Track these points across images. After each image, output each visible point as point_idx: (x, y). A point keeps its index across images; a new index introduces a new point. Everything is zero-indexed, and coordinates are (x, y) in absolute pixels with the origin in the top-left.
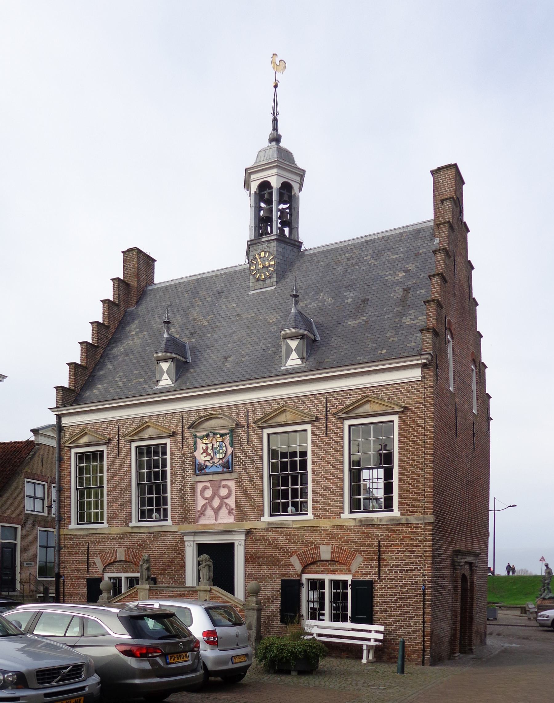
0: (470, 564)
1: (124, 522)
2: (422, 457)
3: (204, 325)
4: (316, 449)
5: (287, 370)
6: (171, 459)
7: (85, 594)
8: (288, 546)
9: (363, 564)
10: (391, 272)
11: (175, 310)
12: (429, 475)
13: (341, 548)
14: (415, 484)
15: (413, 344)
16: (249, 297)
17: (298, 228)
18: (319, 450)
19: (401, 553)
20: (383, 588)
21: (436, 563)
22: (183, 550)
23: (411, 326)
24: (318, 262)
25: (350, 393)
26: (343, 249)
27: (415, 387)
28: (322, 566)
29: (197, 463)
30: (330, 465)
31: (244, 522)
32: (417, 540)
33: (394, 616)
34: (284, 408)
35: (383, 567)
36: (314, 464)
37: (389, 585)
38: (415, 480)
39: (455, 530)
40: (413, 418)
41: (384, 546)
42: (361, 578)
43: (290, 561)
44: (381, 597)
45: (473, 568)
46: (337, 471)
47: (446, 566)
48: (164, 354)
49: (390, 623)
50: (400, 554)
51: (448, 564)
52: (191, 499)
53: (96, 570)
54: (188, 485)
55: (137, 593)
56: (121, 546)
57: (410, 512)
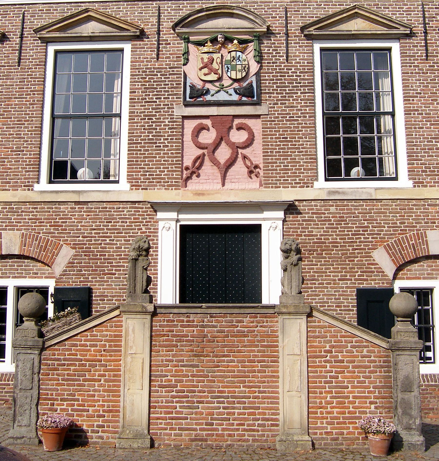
8: (367, 231)
18: (416, 80)
29: (188, 84)
34: (356, 10)
43: (371, 257)
54: (167, 121)
56: (12, 227)
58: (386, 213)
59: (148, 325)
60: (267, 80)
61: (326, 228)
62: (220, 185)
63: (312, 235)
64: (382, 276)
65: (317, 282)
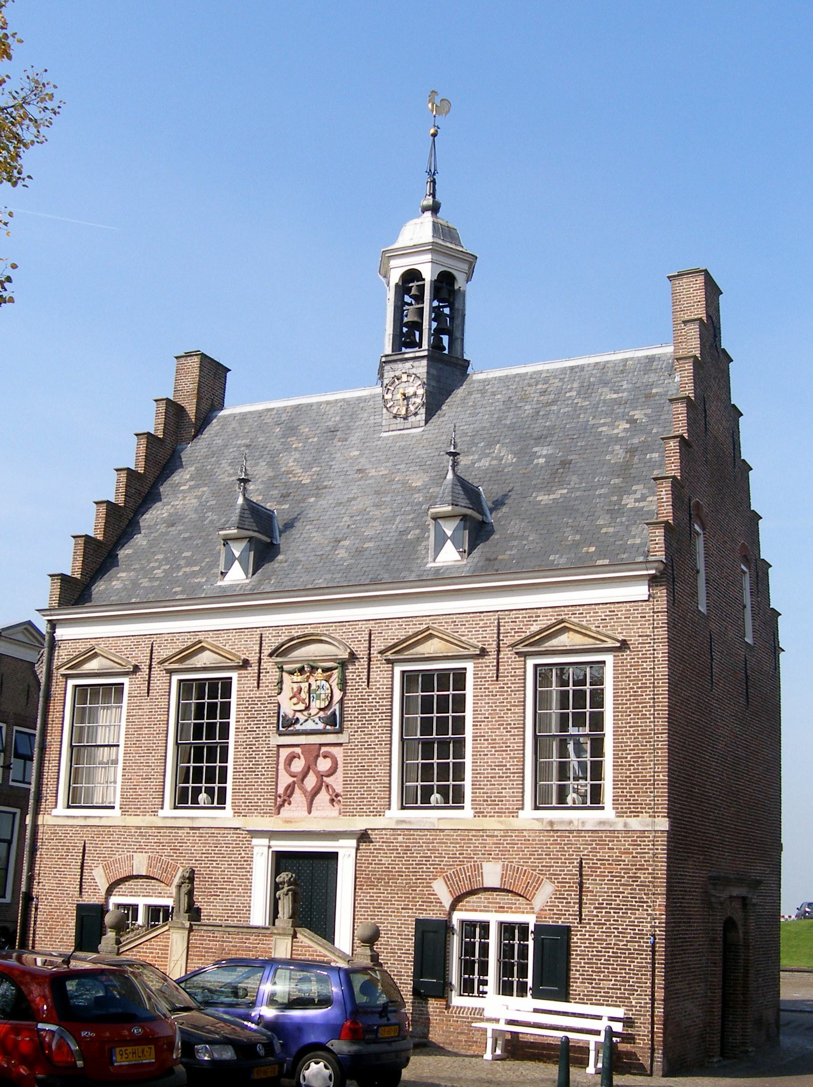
0: (744, 900)
1: (149, 808)
2: (650, 722)
3: (303, 482)
4: (479, 700)
5: (437, 570)
6: (238, 705)
7: (72, 933)
9: (553, 897)
10: (609, 420)
11: (257, 454)
12: (662, 753)
13: (518, 868)
14: (639, 765)
15: (638, 541)
16: (379, 443)
17: (462, 340)
19: (617, 881)
20: (587, 939)
21: (674, 899)
22: (249, 860)
23: (637, 511)
24: (493, 394)
25: (537, 613)
26: (534, 376)
27: (638, 610)
28: (485, 898)
29: (281, 714)
30: (502, 727)
31: (357, 817)
32: (643, 860)
33: (604, 988)
34: (430, 631)
35: (586, 904)
36: (477, 725)
37: (596, 934)
38: (640, 760)
39: (710, 841)
40: (636, 660)
41: (588, 867)
42: (551, 920)
43: (431, 887)
44: (584, 955)
45: (748, 907)
46: (514, 739)
47: (695, 903)
48: (236, 531)
49: (597, 1000)
50: (614, 882)
51: (697, 900)
52: (268, 775)
53: (94, 889)
54: (264, 749)
55: (169, 935)
56: (140, 850)
57: (630, 812)
58: (447, 843)
59: (186, 939)
60: (349, 707)
61: (394, 857)
62: (306, 813)
63: (381, 864)
64: (440, 906)
65: (383, 910)
